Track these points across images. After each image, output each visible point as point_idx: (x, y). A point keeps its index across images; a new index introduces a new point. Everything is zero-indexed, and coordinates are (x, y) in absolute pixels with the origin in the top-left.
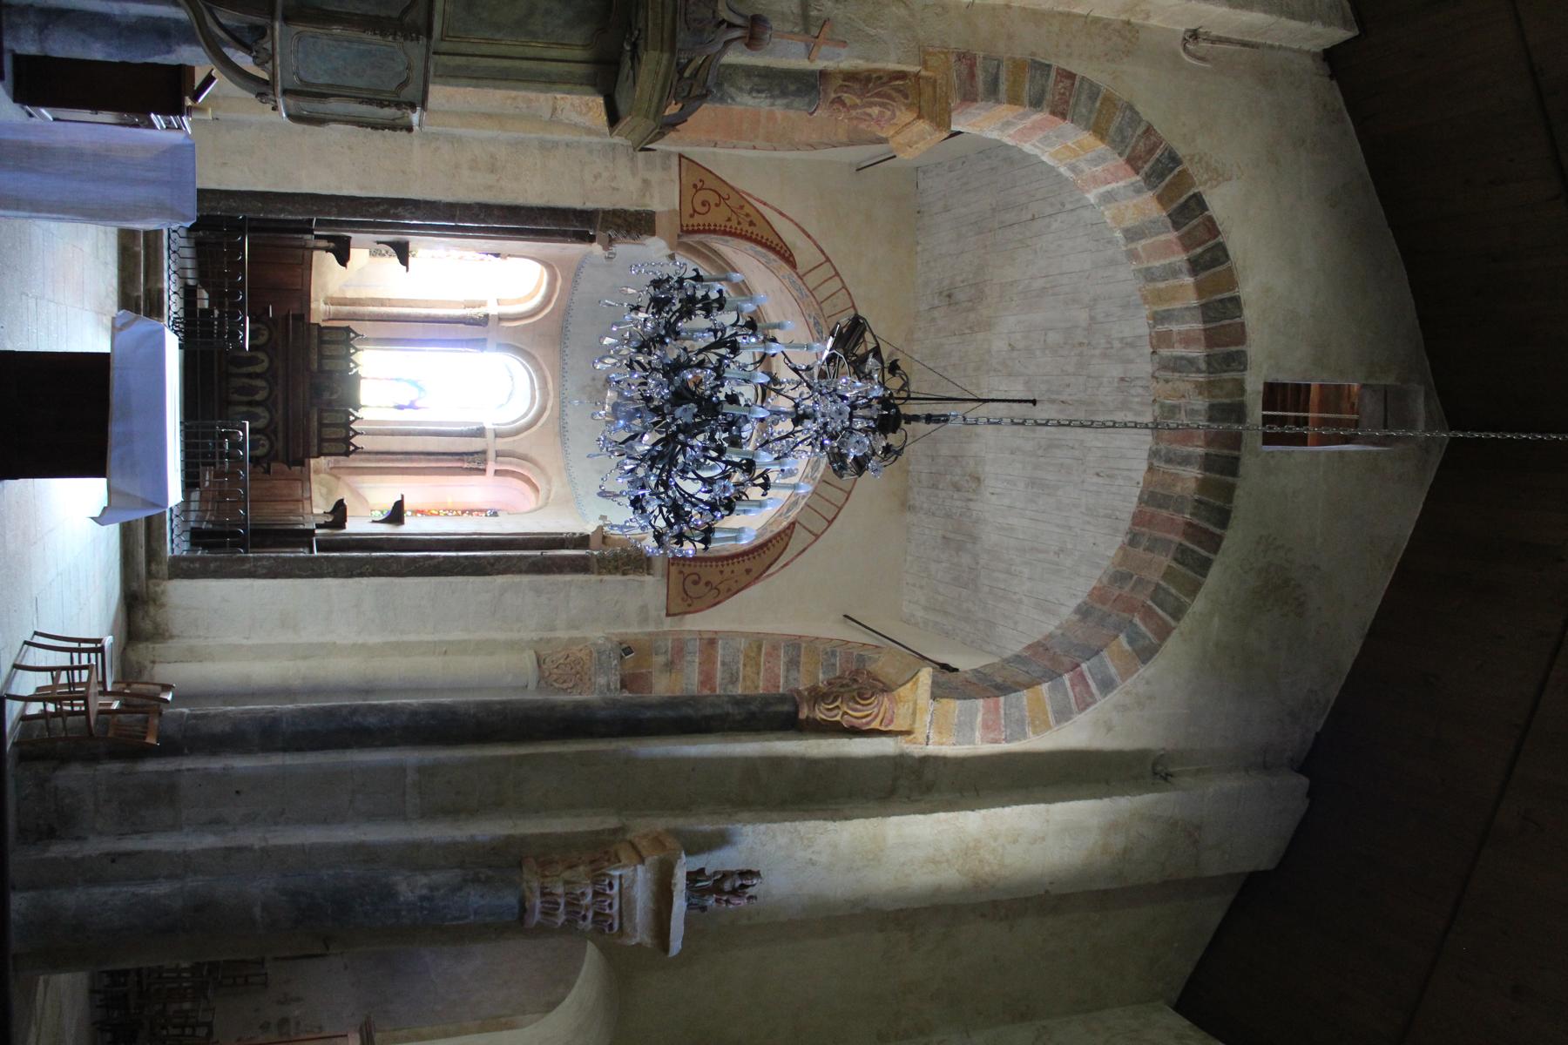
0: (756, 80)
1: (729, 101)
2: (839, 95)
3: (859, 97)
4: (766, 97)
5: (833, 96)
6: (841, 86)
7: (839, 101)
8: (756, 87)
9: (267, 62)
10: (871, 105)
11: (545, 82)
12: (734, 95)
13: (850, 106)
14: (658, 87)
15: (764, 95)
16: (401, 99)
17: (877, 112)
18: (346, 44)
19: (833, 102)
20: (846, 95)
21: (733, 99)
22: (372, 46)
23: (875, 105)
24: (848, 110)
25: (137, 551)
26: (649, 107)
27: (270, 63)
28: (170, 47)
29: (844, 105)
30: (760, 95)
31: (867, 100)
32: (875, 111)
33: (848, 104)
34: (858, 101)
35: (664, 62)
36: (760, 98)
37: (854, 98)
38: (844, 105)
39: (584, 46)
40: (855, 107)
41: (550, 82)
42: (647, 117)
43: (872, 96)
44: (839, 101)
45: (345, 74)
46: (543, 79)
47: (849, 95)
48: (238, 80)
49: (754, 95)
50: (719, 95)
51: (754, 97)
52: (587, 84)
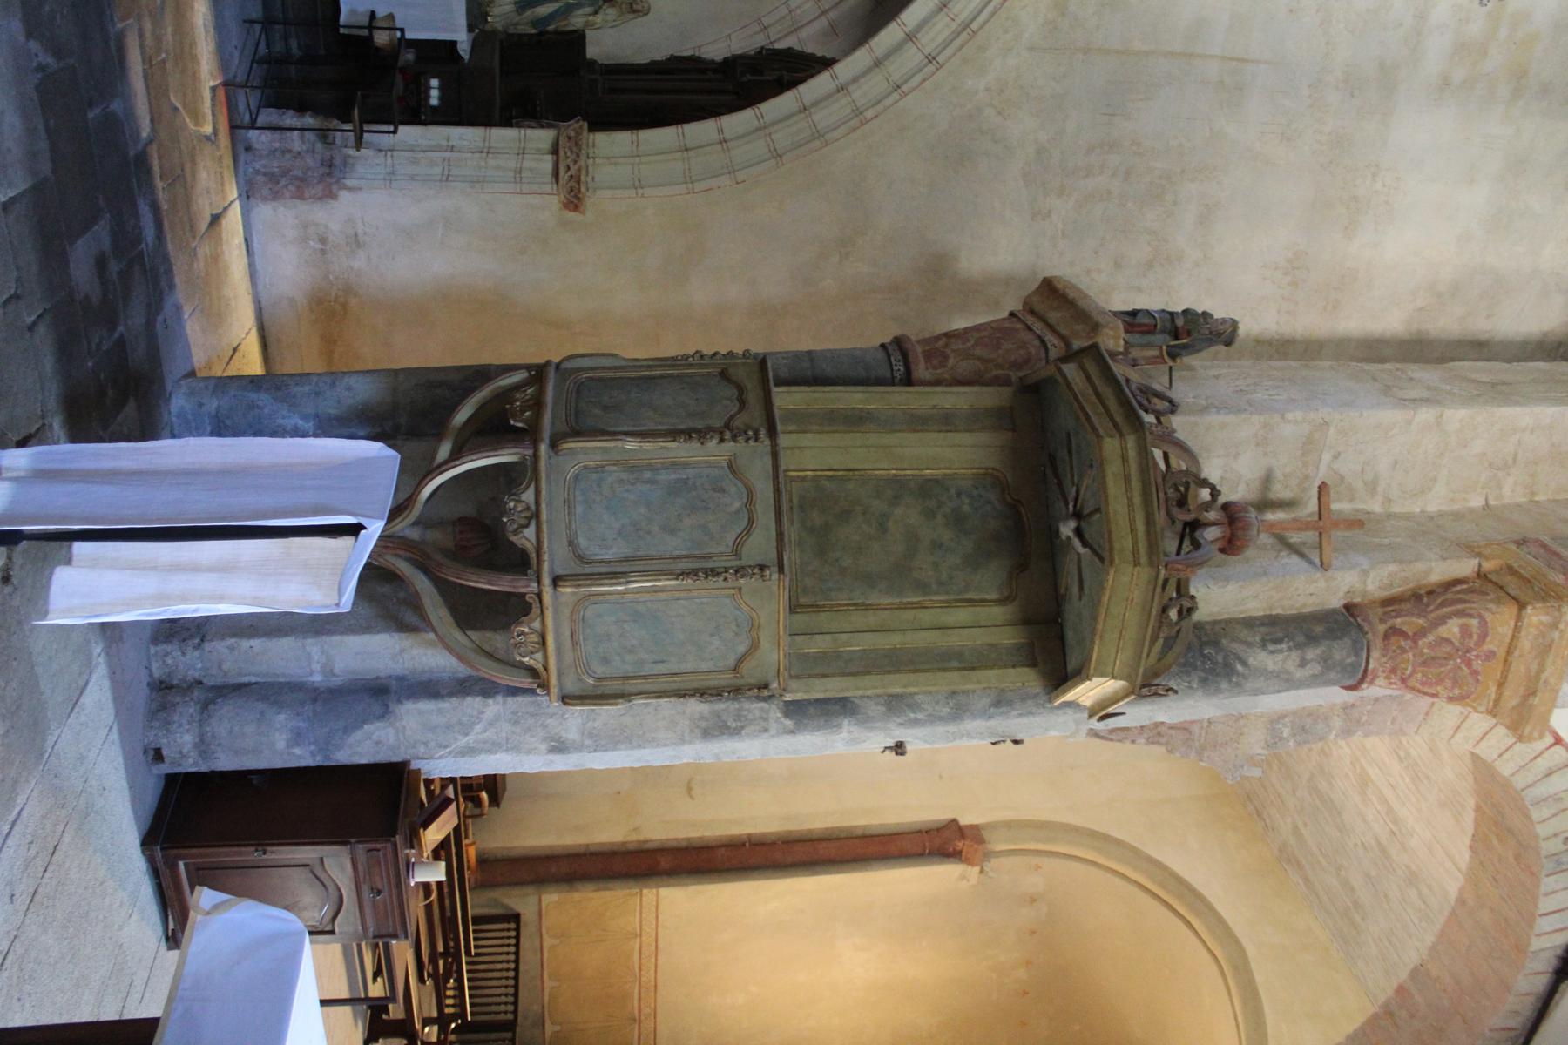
0: (1262, 629)
1: (1239, 667)
2: (1389, 623)
3: (1419, 616)
4: (1290, 649)
5: (1382, 628)
6: (1385, 613)
7: (1394, 632)
8: (1268, 638)
9: (527, 526)
10: (1442, 620)
11: (959, 669)
12: (1242, 654)
13: (1415, 634)
14: (1137, 500)
15: (1284, 646)
16: (744, 562)
17: (1456, 630)
18: (648, 475)
19: (1386, 637)
20: (1399, 620)
21: (1245, 664)
22: (689, 471)
23: (1450, 618)
24: (1415, 642)
25: (192, 7)
26: (1135, 543)
27: (532, 528)
28: (387, 706)
29: (1403, 634)
30: (1279, 647)
31: (1433, 615)
32: (1452, 628)
33: (1410, 634)
34: (1421, 621)
35: (1132, 454)
36: (1281, 651)
37: (1414, 619)
38: (1403, 634)
39: (1002, 601)
40: (1422, 633)
41: (965, 669)
42: (1136, 563)
43: (1437, 608)
44: (1394, 632)
45: (649, 533)
46: (955, 664)
47: (1407, 619)
48: (504, 853)
49: (1271, 647)
50: (1220, 659)
51: (1272, 652)
52: (1023, 666)
